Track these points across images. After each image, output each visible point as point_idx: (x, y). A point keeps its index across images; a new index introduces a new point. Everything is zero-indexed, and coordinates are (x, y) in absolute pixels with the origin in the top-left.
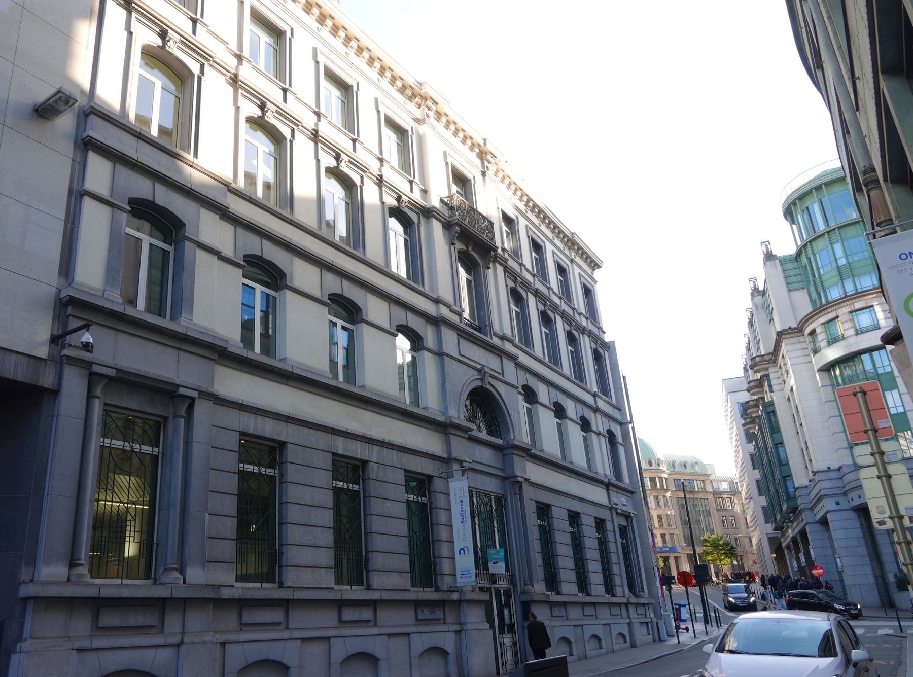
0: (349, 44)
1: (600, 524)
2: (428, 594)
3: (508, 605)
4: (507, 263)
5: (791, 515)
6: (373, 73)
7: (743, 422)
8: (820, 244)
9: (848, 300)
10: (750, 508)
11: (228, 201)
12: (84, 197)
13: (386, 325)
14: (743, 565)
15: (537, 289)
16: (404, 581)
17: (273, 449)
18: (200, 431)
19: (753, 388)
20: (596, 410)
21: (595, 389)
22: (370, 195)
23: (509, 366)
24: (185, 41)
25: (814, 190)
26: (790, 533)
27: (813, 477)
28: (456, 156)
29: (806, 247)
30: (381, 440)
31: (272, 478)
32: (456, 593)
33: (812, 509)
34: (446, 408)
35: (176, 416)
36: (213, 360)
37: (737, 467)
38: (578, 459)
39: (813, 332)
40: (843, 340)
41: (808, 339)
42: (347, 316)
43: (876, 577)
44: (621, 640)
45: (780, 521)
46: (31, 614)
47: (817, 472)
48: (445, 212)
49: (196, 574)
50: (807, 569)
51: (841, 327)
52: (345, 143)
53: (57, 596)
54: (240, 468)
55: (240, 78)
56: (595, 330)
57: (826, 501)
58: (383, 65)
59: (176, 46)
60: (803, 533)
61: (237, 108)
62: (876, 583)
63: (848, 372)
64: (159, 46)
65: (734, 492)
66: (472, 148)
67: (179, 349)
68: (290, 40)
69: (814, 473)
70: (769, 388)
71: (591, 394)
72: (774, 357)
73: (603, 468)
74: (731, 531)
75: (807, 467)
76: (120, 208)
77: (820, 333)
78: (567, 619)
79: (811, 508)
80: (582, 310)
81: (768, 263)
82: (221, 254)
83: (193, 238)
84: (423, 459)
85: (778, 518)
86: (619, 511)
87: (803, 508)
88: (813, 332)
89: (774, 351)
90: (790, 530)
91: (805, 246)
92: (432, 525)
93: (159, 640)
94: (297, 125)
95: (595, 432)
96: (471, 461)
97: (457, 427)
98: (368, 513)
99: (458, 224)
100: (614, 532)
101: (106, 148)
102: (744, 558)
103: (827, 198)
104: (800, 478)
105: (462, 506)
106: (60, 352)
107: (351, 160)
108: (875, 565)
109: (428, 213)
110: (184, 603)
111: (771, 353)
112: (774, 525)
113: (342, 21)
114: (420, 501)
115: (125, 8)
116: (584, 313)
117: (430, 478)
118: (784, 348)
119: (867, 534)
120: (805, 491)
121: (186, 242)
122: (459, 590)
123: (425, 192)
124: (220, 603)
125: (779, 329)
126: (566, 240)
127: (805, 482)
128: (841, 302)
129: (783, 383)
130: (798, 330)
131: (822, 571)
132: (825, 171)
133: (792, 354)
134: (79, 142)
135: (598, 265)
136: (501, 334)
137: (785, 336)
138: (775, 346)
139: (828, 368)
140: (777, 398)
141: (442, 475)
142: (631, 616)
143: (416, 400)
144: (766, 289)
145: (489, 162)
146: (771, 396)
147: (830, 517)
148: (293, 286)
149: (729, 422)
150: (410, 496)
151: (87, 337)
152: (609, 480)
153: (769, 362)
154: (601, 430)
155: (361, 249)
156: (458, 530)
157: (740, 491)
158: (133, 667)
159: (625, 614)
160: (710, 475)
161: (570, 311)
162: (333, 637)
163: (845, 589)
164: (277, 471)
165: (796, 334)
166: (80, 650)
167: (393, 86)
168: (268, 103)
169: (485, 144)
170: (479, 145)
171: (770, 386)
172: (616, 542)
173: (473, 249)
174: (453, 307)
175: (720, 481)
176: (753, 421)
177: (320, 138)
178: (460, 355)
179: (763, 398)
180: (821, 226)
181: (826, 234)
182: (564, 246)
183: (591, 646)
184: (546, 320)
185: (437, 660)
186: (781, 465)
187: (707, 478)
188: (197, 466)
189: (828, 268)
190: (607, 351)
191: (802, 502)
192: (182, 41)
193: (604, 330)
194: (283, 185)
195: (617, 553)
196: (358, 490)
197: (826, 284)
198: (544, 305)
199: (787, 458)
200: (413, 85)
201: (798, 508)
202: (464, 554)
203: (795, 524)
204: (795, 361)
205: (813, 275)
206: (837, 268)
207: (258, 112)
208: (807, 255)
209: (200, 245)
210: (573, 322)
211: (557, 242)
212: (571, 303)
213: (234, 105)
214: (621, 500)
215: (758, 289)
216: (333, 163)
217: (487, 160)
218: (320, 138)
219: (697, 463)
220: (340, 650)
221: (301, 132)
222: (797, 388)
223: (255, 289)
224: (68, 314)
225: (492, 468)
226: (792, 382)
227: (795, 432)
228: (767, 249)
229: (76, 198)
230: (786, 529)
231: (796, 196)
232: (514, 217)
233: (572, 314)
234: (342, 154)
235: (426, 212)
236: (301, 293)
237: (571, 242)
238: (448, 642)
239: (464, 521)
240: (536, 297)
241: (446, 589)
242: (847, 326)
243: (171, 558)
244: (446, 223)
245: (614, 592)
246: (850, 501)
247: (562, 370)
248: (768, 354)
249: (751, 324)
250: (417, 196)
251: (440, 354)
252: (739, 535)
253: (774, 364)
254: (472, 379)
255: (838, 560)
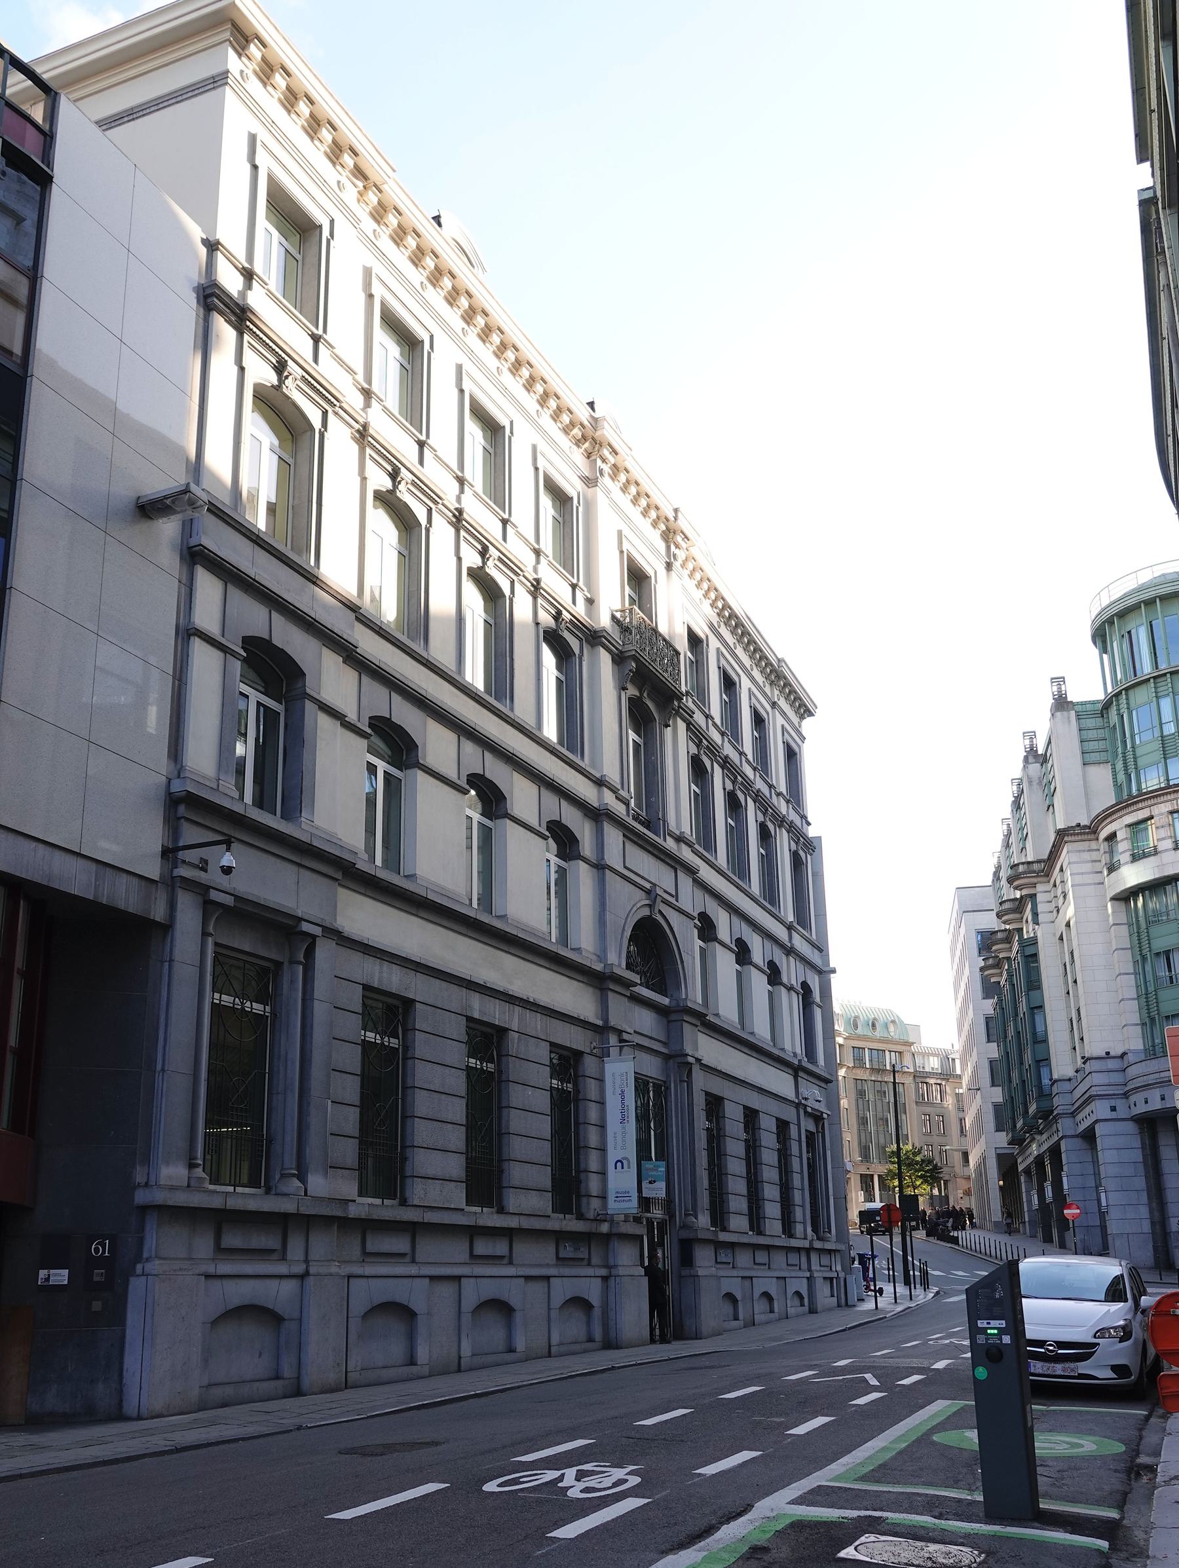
0: (502, 354)
1: (783, 1126)
2: (571, 1224)
3: (661, 1244)
4: (692, 717)
5: (1040, 1121)
6: (453, 317)
7: (983, 964)
8: (1141, 696)
9: (1170, 793)
10: (974, 1105)
11: (357, 637)
12: (192, 638)
13: (452, 774)
14: (947, 1197)
15: (727, 757)
16: (457, 1195)
17: (265, 971)
18: (322, 985)
19: (1007, 912)
20: (790, 951)
21: (791, 918)
22: (522, 608)
23: (685, 882)
24: (307, 376)
25: (1142, 605)
26: (1034, 1150)
27: (1083, 1066)
28: (636, 542)
29: (1120, 697)
30: (525, 998)
31: (260, 1018)
32: (606, 1223)
33: (1073, 1114)
34: (604, 950)
35: (293, 962)
36: (336, 880)
37: (960, 1035)
38: (761, 1029)
39: (1112, 837)
40: (1154, 855)
41: (1104, 846)
42: (390, 753)
43: (1153, 1224)
44: (797, 1302)
45: (1022, 1129)
46: (155, 1226)
47: (1089, 1059)
48: (616, 635)
49: (318, 1184)
50: (1053, 1208)
51: (1154, 835)
52: (405, 448)
53: (185, 1205)
54: (215, 1001)
55: (371, 431)
56: (797, 821)
57: (1097, 1105)
58: (533, 374)
59: (295, 385)
60: (1055, 1152)
61: (364, 479)
62: (1153, 1233)
63: (1154, 904)
64: (273, 386)
65: (947, 1075)
66: (655, 524)
67: (299, 865)
68: (429, 354)
69: (1086, 1060)
70: (1033, 916)
71: (784, 926)
72: (1048, 865)
73: (792, 1043)
74: (936, 1140)
75: (1074, 1048)
76: (234, 654)
77: (1122, 840)
78: (733, 1267)
79: (1072, 1113)
80: (783, 788)
81: (1058, 714)
82: (346, 719)
83: (316, 696)
84: (573, 1026)
85: (1019, 1124)
86: (809, 1110)
87: (1061, 1112)
88: (1112, 837)
89: (1049, 858)
90: (1035, 1145)
91: (1118, 695)
92: (405, 1088)
93: (282, 1269)
94: (333, 405)
95: (785, 986)
96: (632, 1032)
97: (619, 980)
98: (581, 1120)
99: (634, 658)
100: (800, 1141)
101: (219, 562)
102: (950, 1185)
103: (1160, 620)
104: (1062, 1065)
105: (623, 1099)
106: (172, 871)
107: (416, 480)
108: (1154, 1205)
109: (594, 638)
110: (306, 1222)
111: (1043, 861)
112: (1010, 1135)
113: (529, 354)
114: (386, 1044)
115: (235, 328)
116: (785, 793)
117: (578, 1055)
118: (1065, 857)
119: (1149, 1157)
120: (1067, 1086)
121: (306, 701)
122: (608, 1219)
123: (590, 602)
124: (344, 1224)
125: (1061, 826)
126: (768, 670)
127: (1070, 1073)
128: (1160, 795)
129: (1055, 912)
130: (1090, 831)
131: (1078, 1211)
132: (1164, 575)
133: (1077, 868)
134: (185, 552)
135: (810, 711)
136: (678, 833)
137: (1070, 838)
138: (1051, 852)
139: (1127, 897)
140: (1044, 935)
141: (595, 1051)
142: (813, 1268)
143: (486, 899)
144: (1048, 755)
145: (677, 546)
146: (1034, 929)
147: (1099, 1130)
148: (427, 765)
149: (957, 960)
150: (368, 1034)
151: (228, 859)
152: (800, 1061)
153: (1038, 874)
154: (794, 982)
155: (422, 641)
156: (615, 1134)
157: (958, 1072)
158: (257, 1302)
159: (804, 1265)
160: (913, 1043)
161: (765, 790)
162: (464, 1277)
163: (1107, 1240)
164: (268, 1009)
165: (1086, 837)
166: (208, 1276)
167: (555, 421)
168: (403, 469)
169: (676, 518)
170: (667, 520)
171: (1035, 914)
172: (801, 1157)
173: (648, 694)
174: (621, 792)
175: (926, 1054)
176: (998, 965)
177: (464, 523)
178: (625, 867)
179: (1020, 930)
180: (1146, 668)
181: (1152, 680)
182: (735, 641)
183: (760, 1306)
184: (734, 805)
185: (578, 1315)
186: (1036, 1041)
187: (908, 1048)
188: (319, 1036)
189: (1147, 736)
190: (811, 855)
191: (1060, 1103)
192: (303, 377)
193: (809, 819)
194: (414, 601)
195: (802, 1173)
196: (397, 1046)
197: (1140, 762)
198: (698, 746)
199: (1046, 1031)
200: (586, 423)
201: (1052, 1112)
202: (623, 1168)
203: (1045, 1136)
204: (1079, 879)
205: (1124, 743)
206: (1160, 738)
207: (388, 484)
208: (1118, 710)
209: (323, 706)
210: (769, 809)
211: (756, 673)
212: (768, 777)
213: (359, 475)
214: (812, 1093)
215: (1037, 750)
216: (386, 483)
217: (601, 457)
218: (464, 523)
219: (893, 1022)
220: (472, 1294)
221: (441, 512)
222: (1076, 922)
223: (247, 697)
224: (179, 815)
225: (653, 1042)
226: (1070, 912)
227: (1064, 992)
228: (1060, 691)
229: (183, 639)
230: (1029, 1143)
231: (1115, 610)
232: (703, 636)
233: (768, 796)
234: (491, 547)
235: (591, 635)
236: (435, 774)
237: (776, 674)
238: (593, 1292)
239: (625, 1121)
240: (723, 769)
241: (592, 1217)
242: (1163, 833)
243: (290, 1161)
244: (617, 655)
245: (793, 1232)
246: (1132, 1106)
247: (750, 887)
248: (1039, 862)
249: (1017, 805)
250: (580, 610)
251: (600, 867)
252: (947, 1147)
253: (1045, 879)
254: (639, 905)
255: (1103, 1195)
